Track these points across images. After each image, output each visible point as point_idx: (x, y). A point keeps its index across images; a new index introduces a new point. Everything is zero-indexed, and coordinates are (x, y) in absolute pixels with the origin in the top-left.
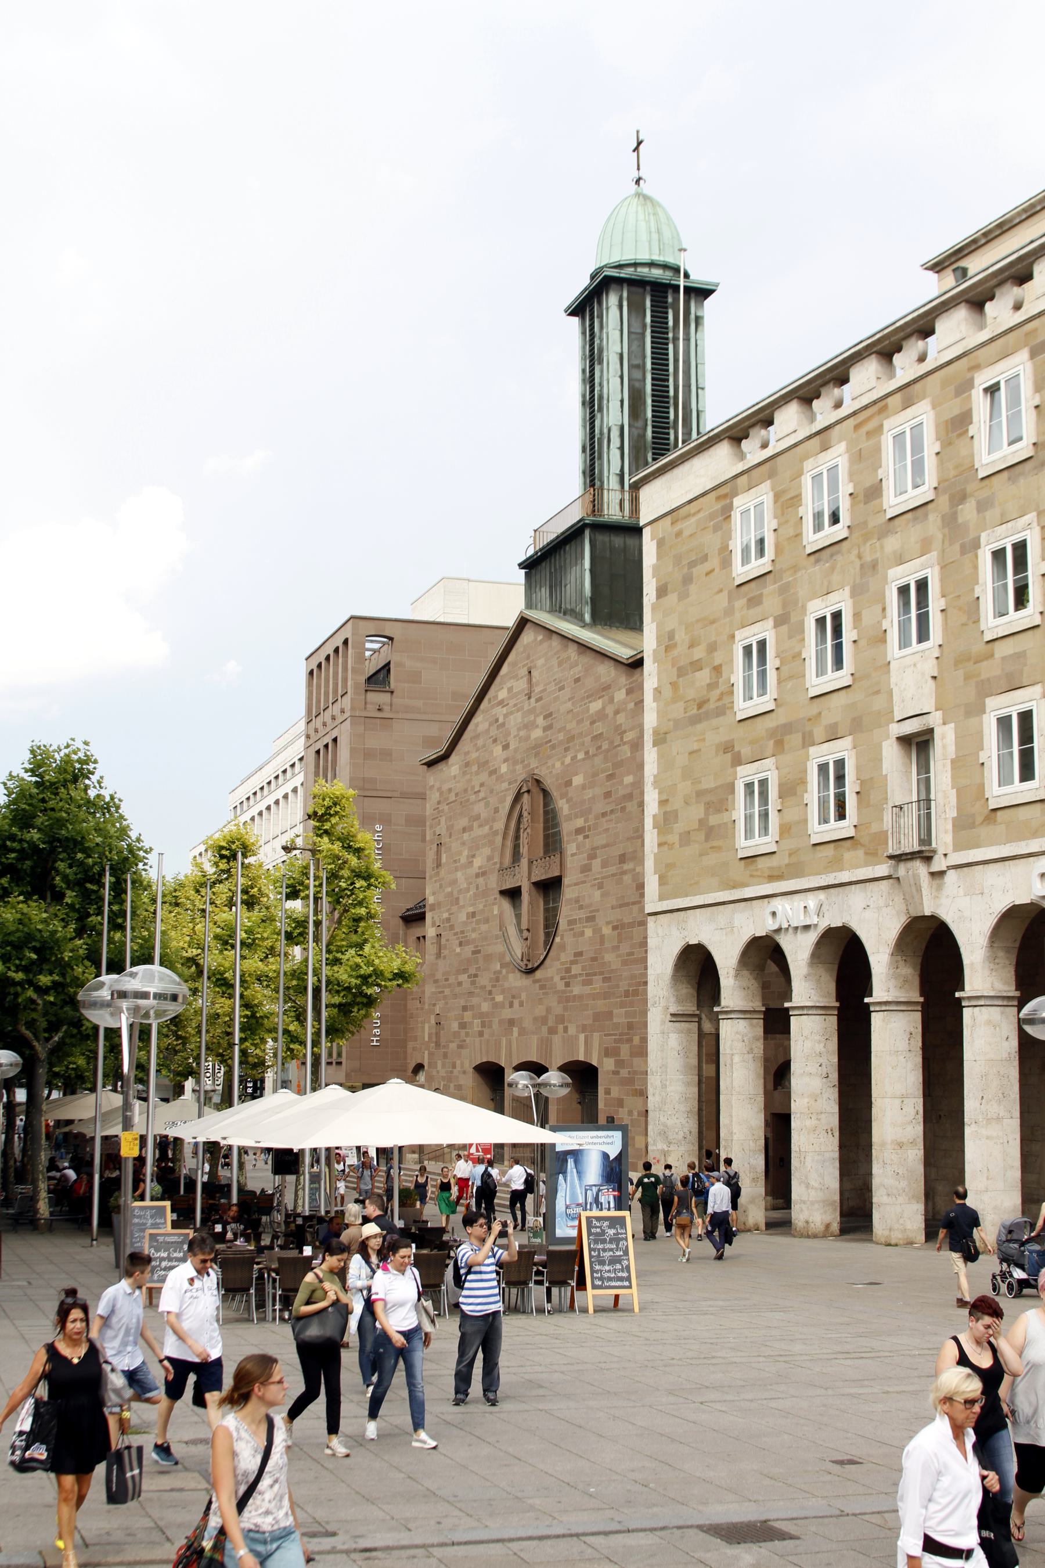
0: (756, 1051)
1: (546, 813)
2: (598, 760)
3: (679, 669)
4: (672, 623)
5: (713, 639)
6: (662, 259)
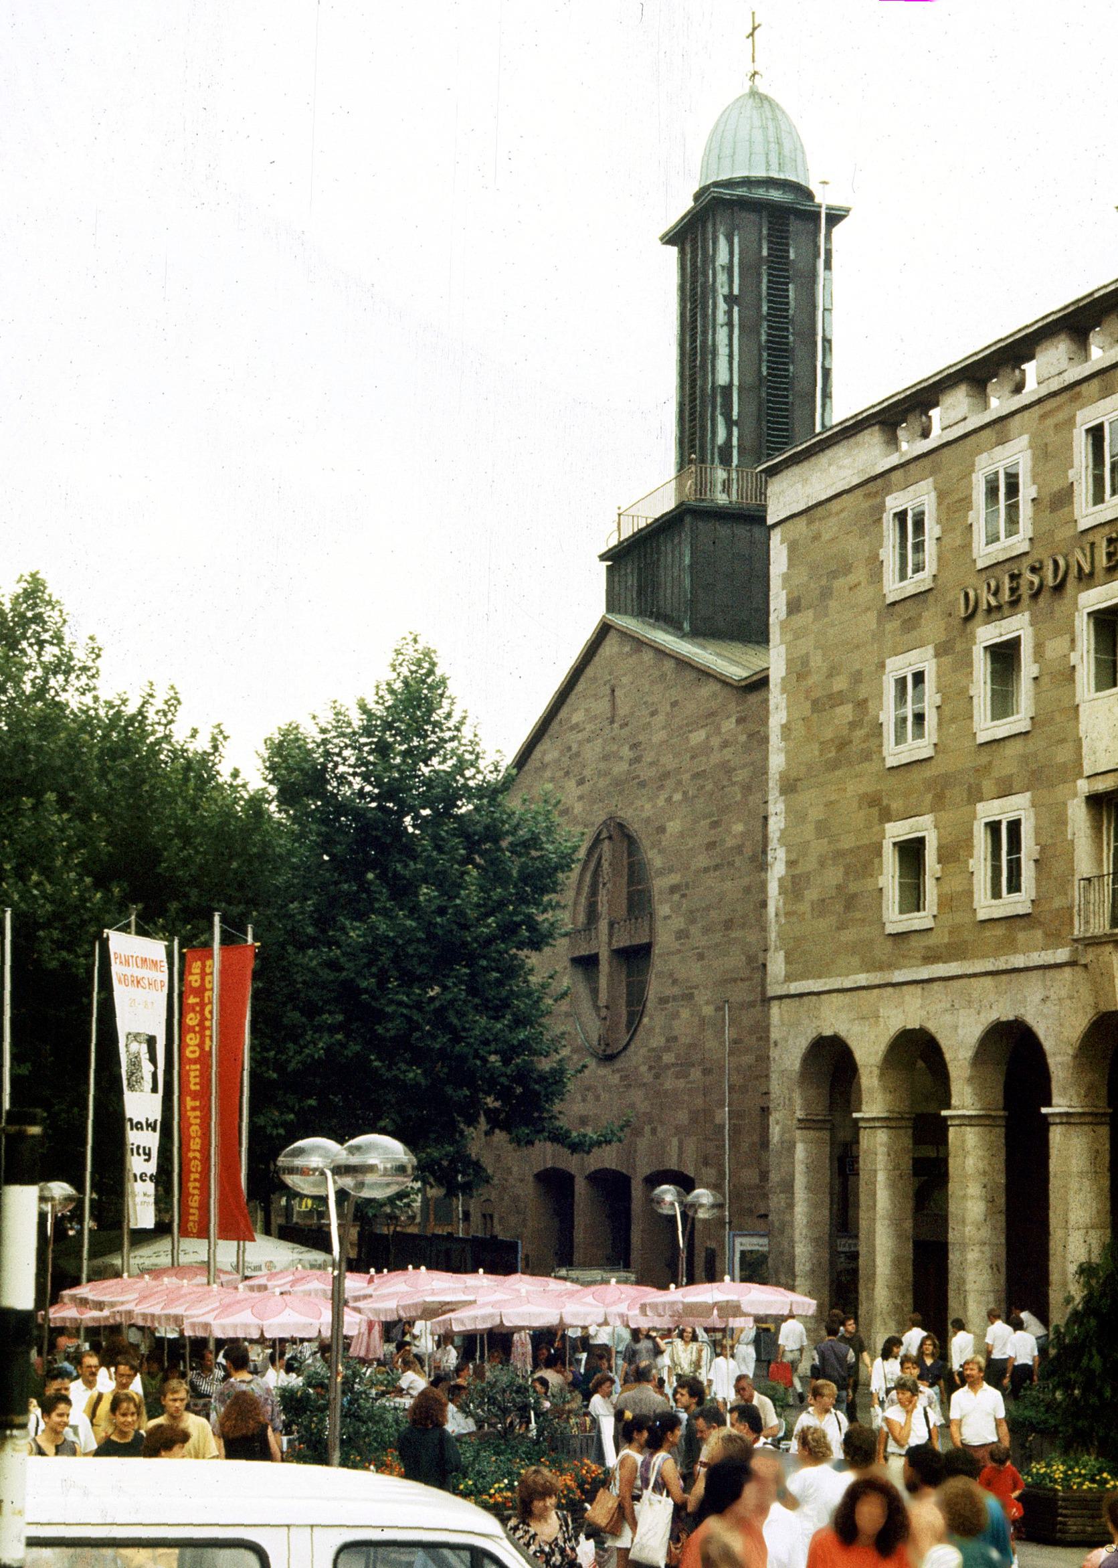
0: (903, 1167)
1: (631, 866)
2: (700, 804)
3: (815, 702)
4: (806, 645)
5: (858, 667)
6: (782, 177)
